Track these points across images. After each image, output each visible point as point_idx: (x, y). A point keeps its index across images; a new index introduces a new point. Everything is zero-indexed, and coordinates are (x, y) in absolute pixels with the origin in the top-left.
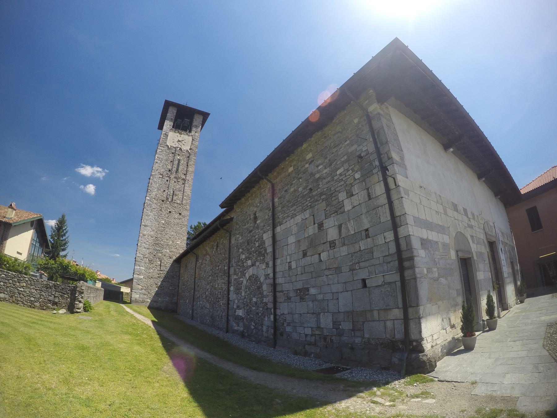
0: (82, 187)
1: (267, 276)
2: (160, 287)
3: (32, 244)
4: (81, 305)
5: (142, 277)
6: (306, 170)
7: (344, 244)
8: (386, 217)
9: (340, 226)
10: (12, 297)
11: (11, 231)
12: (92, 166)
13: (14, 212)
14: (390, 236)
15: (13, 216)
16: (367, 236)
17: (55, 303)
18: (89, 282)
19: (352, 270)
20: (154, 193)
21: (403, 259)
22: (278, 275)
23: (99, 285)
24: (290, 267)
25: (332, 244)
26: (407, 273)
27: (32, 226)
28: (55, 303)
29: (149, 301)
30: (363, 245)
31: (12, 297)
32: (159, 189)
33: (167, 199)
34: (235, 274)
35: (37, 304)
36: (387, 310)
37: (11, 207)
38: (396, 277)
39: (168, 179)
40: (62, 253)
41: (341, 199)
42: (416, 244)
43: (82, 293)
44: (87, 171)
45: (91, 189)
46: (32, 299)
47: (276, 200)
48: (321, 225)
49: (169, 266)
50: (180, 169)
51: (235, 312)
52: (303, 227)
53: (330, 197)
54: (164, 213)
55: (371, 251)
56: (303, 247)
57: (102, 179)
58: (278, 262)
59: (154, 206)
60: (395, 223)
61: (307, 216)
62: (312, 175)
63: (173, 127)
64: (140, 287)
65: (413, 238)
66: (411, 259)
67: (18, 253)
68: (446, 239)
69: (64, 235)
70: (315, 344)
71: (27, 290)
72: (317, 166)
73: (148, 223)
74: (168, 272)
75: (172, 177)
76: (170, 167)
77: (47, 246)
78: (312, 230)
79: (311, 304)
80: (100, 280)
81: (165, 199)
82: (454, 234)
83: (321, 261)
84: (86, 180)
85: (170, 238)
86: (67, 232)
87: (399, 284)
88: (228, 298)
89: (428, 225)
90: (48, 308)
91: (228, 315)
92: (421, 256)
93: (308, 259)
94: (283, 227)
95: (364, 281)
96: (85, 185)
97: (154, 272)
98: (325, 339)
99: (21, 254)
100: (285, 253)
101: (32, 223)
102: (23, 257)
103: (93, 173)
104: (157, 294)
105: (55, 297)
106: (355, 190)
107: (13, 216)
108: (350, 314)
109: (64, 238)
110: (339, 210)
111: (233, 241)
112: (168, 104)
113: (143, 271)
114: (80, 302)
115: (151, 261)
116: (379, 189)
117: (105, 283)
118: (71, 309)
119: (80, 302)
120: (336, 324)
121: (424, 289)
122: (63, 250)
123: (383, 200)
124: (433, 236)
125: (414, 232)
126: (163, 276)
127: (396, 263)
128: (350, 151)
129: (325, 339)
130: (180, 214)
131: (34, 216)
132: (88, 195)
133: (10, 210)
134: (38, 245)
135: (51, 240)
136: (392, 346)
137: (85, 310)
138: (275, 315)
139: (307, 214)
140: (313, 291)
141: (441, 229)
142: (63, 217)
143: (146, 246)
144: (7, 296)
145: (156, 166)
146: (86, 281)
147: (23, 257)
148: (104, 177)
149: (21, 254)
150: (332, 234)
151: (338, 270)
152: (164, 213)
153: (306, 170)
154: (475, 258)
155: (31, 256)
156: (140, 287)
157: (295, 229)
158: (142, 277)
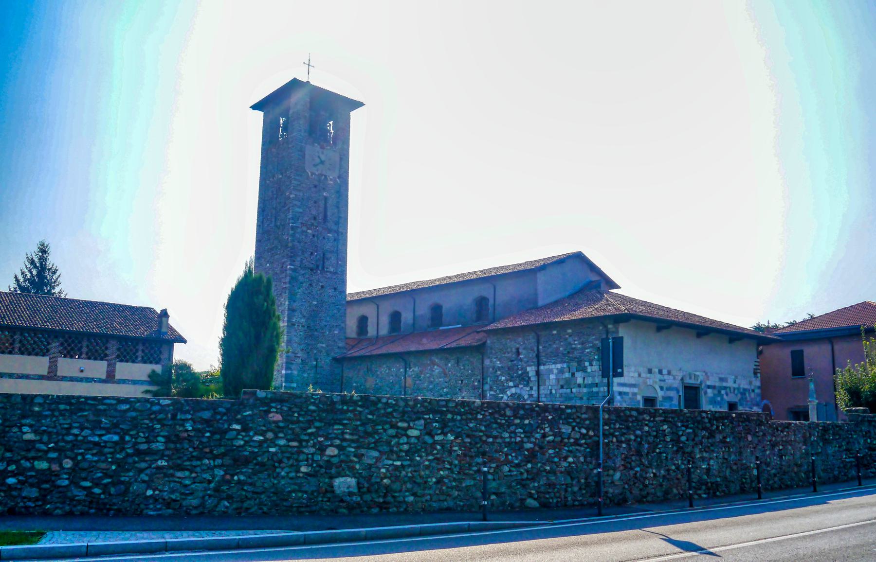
1: (531, 396)
6: (566, 339)
19: (588, 399)
24: (551, 393)
25: (579, 386)
30: (595, 389)
34: (491, 389)
48: (573, 374)
50: (329, 214)
52: (561, 371)
53: (580, 362)
55: (597, 393)
56: (561, 383)
58: (541, 388)
62: (570, 344)
68: (636, 390)
78: (567, 375)
93: (564, 391)
94: (546, 367)
100: (547, 383)
106: (594, 363)
110: (584, 370)
111: (487, 362)
130: (335, 289)
139: (565, 365)
142: (361, 104)
150: (580, 381)
151: (581, 399)
153: (566, 339)
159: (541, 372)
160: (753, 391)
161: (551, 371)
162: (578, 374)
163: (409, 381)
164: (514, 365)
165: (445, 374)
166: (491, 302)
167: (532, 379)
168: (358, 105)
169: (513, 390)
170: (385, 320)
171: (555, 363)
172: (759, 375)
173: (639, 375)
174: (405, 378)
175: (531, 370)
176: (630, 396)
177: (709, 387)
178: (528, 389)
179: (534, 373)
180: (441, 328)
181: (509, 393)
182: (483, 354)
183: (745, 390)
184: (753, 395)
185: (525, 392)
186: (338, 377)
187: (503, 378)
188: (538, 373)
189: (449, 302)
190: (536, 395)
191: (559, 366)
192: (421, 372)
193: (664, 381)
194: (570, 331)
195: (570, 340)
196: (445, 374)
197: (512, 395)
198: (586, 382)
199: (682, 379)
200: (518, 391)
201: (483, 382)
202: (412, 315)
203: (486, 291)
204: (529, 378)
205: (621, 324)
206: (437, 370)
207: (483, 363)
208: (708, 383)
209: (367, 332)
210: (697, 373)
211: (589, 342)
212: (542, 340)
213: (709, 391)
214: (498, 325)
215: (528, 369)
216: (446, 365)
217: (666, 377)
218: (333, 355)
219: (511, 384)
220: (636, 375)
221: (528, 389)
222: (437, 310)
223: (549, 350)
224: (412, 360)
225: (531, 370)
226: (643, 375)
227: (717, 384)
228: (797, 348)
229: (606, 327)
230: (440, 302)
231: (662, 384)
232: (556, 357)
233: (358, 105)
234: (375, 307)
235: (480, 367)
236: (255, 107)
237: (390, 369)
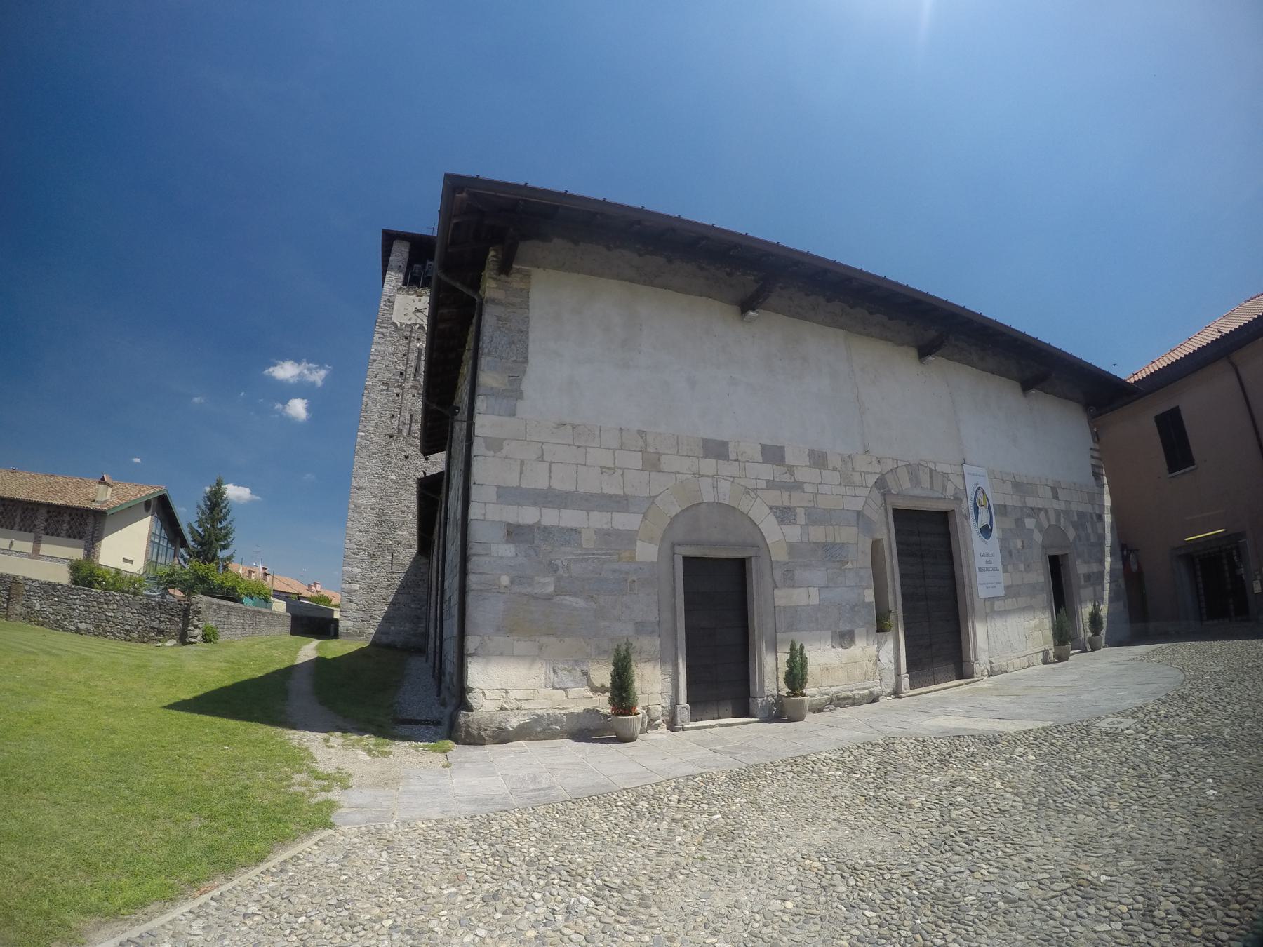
0: (278, 406)
2: (393, 605)
3: (151, 543)
4: (198, 632)
5: (357, 587)
10: (97, 627)
11: (108, 524)
12: (298, 361)
13: (110, 489)
15: (108, 497)
17: (161, 632)
18: (247, 600)
20: (373, 423)
23: (279, 606)
27: (147, 509)
28: (161, 632)
29: (373, 631)
31: (97, 627)
32: (381, 414)
33: (400, 431)
35: (135, 635)
37: (102, 481)
39: (399, 390)
40: (222, 554)
43: (199, 613)
44: (286, 371)
45: (298, 408)
46: (127, 627)
49: (408, 562)
54: (395, 459)
57: (319, 383)
59: (374, 448)
63: (405, 284)
64: (354, 606)
67: (125, 560)
69: (225, 518)
71: (119, 615)
73: (364, 482)
74: (407, 575)
75: (407, 385)
76: (402, 367)
77: (184, 543)
80: (279, 595)
81: (395, 433)
84: (287, 391)
86: (229, 511)
90: (151, 639)
96: (285, 402)
97: (381, 576)
99: (131, 562)
101: (147, 505)
102: (137, 567)
103: (300, 375)
104: (387, 618)
105: (161, 622)
107: (108, 497)
109: (224, 523)
112: (389, 238)
113: (359, 576)
114: (196, 627)
115: (372, 556)
117: (293, 601)
118: (183, 639)
119: (196, 627)
122: (225, 547)
126: (398, 582)
131: (150, 491)
132: (290, 422)
133: (102, 487)
134: (164, 542)
135: (200, 530)
137: (206, 639)
141: (620, 503)
143: (362, 527)
144: (90, 627)
145: (373, 368)
146: (239, 600)
147: (137, 567)
148: (325, 380)
149: (131, 562)
152: (395, 459)
155: (150, 563)
156: (354, 606)
158: (357, 587)
183: (1081, 515)
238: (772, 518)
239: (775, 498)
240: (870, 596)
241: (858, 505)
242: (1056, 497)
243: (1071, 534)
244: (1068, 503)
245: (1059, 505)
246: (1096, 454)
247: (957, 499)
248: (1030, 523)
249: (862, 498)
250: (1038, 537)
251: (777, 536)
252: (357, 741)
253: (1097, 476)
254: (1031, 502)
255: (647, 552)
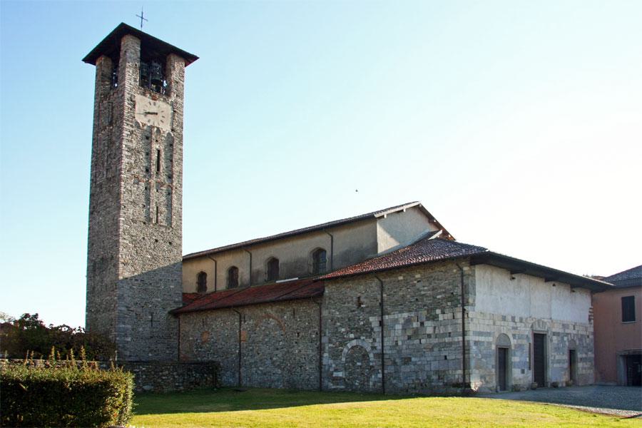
1: (374, 348)
6: (414, 285)
7: (436, 337)
8: (460, 330)
9: (435, 328)
14: (461, 338)
16: (450, 336)
21: (465, 349)
22: (385, 348)
24: (397, 344)
25: (429, 336)
26: (466, 356)
34: (330, 342)
36: (456, 369)
38: (462, 357)
41: (437, 313)
42: (472, 344)
47: (384, 295)
48: (422, 324)
51: (332, 374)
52: (408, 321)
58: (386, 339)
60: (464, 334)
61: (413, 315)
65: (471, 342)
66: (469, 350)
68: (491, 339)
70: (415, 388)
72: (424, 287)
78: (415, 325)
79: (413, 367)
82: (497, 336)
83: (420, 343)
85: (161, 280)
87: (462, 360)
88: (321, 363)
89: (480, 334)
91: (321, 377)
92: (474, 348)
94: (391, 317)
95: (446, 357)
98: (422, 385)
106: (446, 311)
108: (437, 372)
110: (435, 318)
111: (325, 313)
116: (459, 315)
120: (429, 377)
121: (473, 363)
123: (460, 321)
124: (482, 339)
125: (471, 338)
127: (462, 351)
128: (447, 287)
129: (422, 385)
130: (170, 243)
136: (457, 385)
138: (383, 374)
140: (413, 359)
141: (488, 334)
150: (429, 330)
154: (513, 348)
157: (402, 321)
159: (385, 323)
160: (588, 337)
161: (396, 321)
162: (428, 324)
163: (244, 334)
164: (356, 315)
165: (281, 326)
166: (328, 254)
167: (375, 330)
168: (189, 58)
169: (354, 343)
170: (223, 275)
171: (401, 312)
172: (592, 321)
173: (494, 324)
174: (240, 331)
175: (374, 321)
176: (485, 344)
177: (554, 334)
178: (371, 341)
179: (377, 324)
180: (277, 282)
181: (349, 346)
182: (320, 304)
183: (582, 335)
184: (588, 340)
185: (367, 344)
186: (175, 331)
187: (343, 330)
188: (381, 324)
189: (284, 254)
190: (380, 348)
191: (406, 315)
192: (256, 325)
193: (516, 328)
194: (418, 276)
195: (419, 285)
196: (281, 326)
197: (353, 348)
198: (437, 331)
199: (532, 326)
200: (360, 343)
201: (320, 334)
202: (249, 268)
203: (322, 241)
204: (372, 329)
205: (476, 266)
206: (273, 322)
207: (321, 314)
208: (554, 330)
209: (206, 288)
210: (546, 320)
211: (441, 288)
212: (386, 287)
213: (555, 338)
214: (330, 275)
215: (371, 319)
216: (282, 317)
217: (519, 325)
218: (169, 309)
219: (352, 336)
220: (491, 322)
221: (371, 341)
222: (273, 262)
223: (396, 298)
224: (247, 312)
225: (374, 321)
226: (498, 323)
227: (561, 331)
228: (627, 294)
229: (461, 269)
230: (276, 255)
231: (516, 332)
232: (401, 305)
233: (189, 58)
234: (214, 263)
235: (318, 318)
236: (90, 59)
237: (225, 323)
238: (477, 340)
239: (513, 332)
240: (528, 360)
241: (527, 333)
242: (574, 329)
243: (577, 342)
244: (578, 331)
245: (575, 332)
246: (591, 310)
247: (548, 331)
248: (565, 339)
249: (527, 331)
250: (567, 344)
251: (513, 342)
252: (136, 82)
253: (590, 320)
254: (567, 331)
255: (493, 347)
